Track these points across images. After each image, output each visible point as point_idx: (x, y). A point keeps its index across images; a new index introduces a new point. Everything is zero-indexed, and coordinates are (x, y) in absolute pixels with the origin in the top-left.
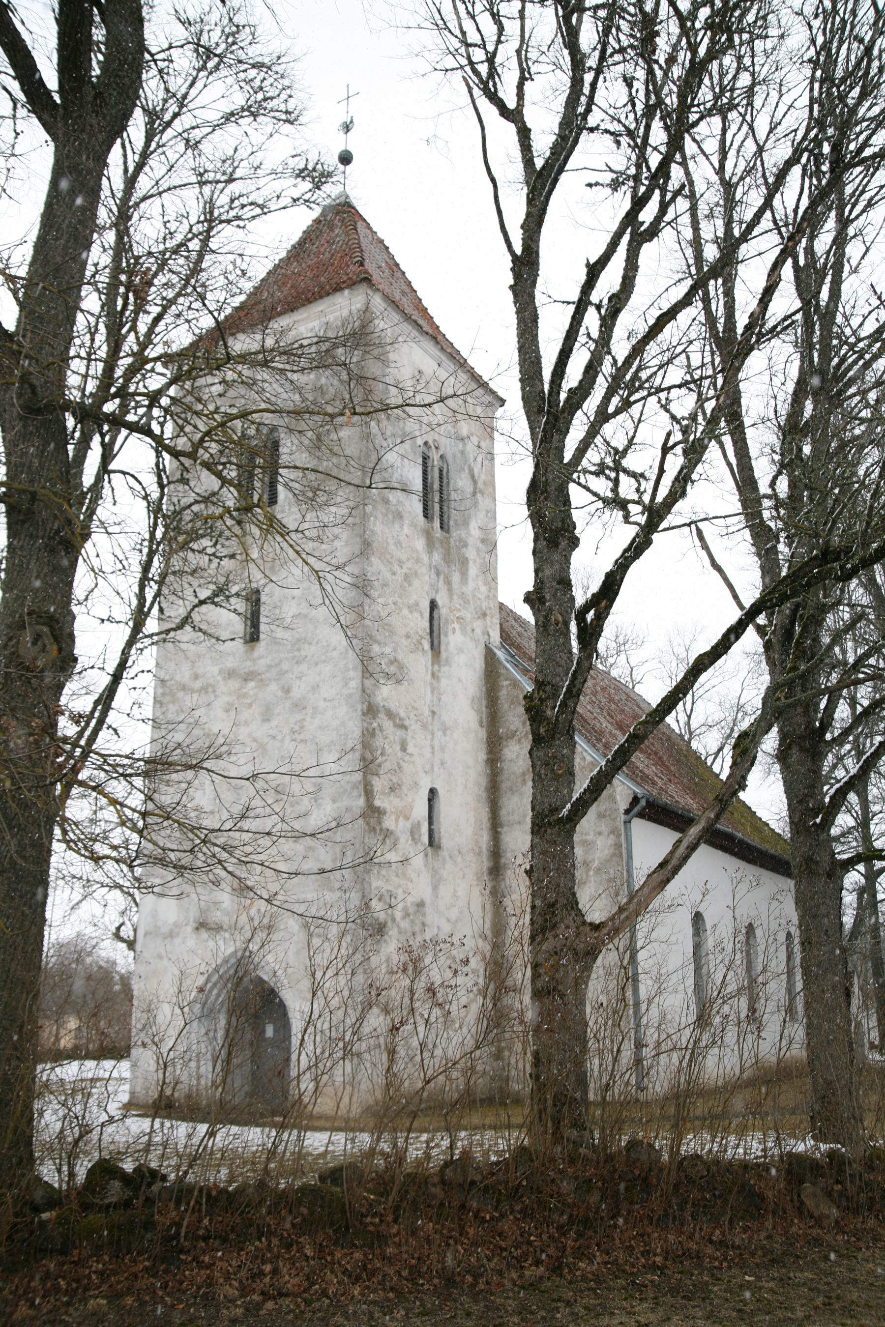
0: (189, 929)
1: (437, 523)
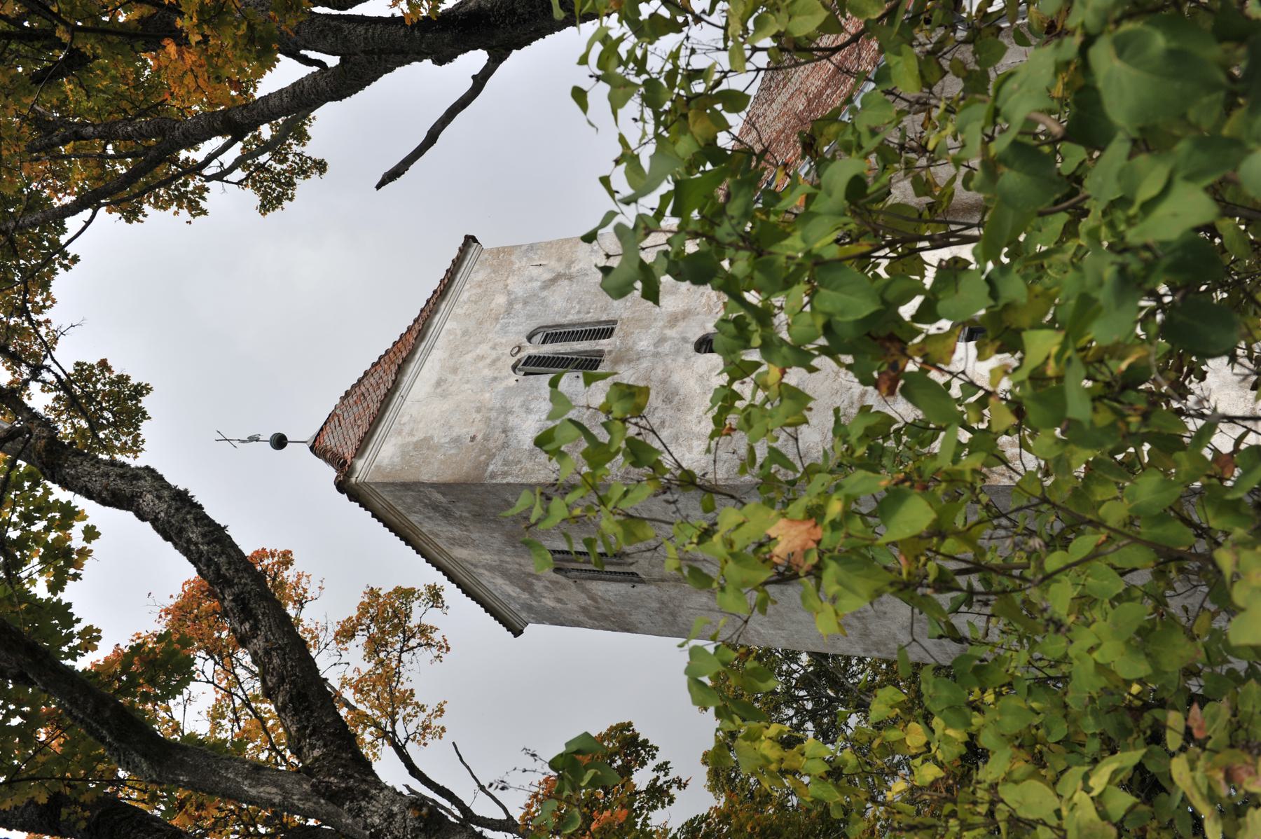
1: (603, 344)
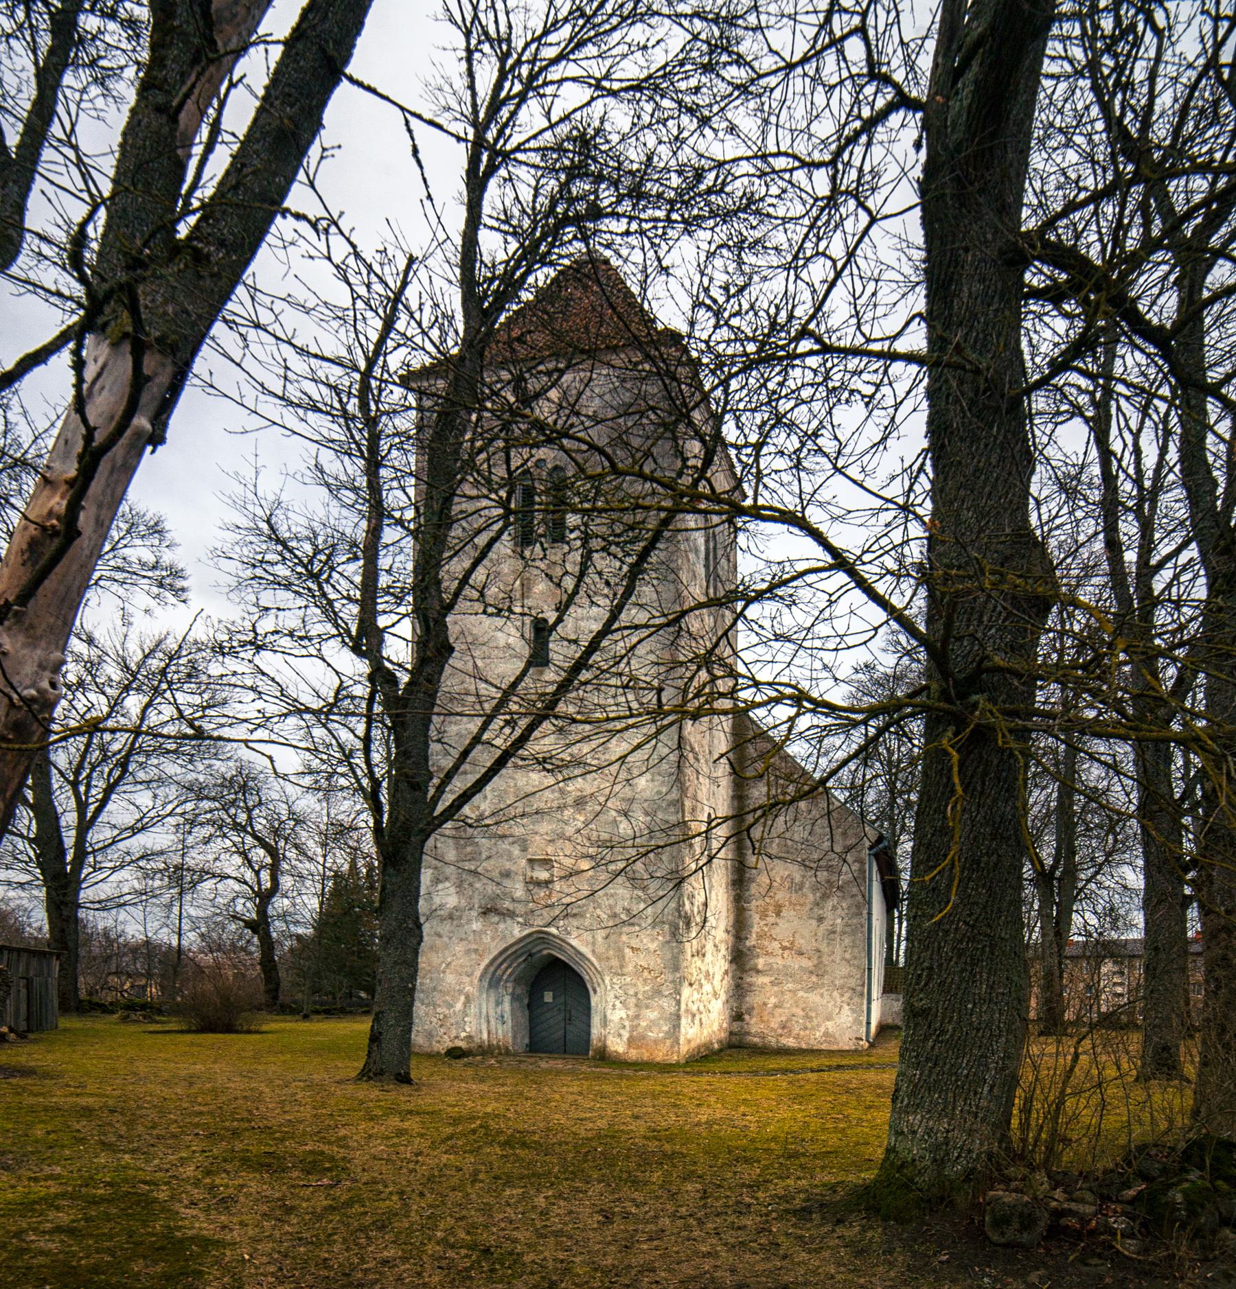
0: (474, 914)
